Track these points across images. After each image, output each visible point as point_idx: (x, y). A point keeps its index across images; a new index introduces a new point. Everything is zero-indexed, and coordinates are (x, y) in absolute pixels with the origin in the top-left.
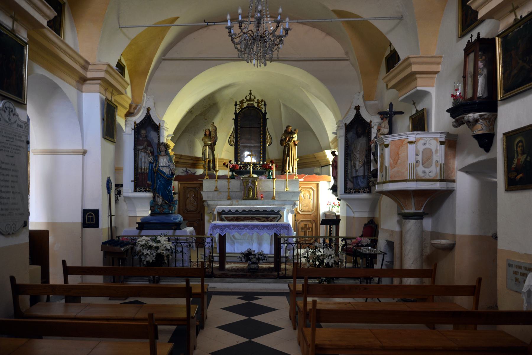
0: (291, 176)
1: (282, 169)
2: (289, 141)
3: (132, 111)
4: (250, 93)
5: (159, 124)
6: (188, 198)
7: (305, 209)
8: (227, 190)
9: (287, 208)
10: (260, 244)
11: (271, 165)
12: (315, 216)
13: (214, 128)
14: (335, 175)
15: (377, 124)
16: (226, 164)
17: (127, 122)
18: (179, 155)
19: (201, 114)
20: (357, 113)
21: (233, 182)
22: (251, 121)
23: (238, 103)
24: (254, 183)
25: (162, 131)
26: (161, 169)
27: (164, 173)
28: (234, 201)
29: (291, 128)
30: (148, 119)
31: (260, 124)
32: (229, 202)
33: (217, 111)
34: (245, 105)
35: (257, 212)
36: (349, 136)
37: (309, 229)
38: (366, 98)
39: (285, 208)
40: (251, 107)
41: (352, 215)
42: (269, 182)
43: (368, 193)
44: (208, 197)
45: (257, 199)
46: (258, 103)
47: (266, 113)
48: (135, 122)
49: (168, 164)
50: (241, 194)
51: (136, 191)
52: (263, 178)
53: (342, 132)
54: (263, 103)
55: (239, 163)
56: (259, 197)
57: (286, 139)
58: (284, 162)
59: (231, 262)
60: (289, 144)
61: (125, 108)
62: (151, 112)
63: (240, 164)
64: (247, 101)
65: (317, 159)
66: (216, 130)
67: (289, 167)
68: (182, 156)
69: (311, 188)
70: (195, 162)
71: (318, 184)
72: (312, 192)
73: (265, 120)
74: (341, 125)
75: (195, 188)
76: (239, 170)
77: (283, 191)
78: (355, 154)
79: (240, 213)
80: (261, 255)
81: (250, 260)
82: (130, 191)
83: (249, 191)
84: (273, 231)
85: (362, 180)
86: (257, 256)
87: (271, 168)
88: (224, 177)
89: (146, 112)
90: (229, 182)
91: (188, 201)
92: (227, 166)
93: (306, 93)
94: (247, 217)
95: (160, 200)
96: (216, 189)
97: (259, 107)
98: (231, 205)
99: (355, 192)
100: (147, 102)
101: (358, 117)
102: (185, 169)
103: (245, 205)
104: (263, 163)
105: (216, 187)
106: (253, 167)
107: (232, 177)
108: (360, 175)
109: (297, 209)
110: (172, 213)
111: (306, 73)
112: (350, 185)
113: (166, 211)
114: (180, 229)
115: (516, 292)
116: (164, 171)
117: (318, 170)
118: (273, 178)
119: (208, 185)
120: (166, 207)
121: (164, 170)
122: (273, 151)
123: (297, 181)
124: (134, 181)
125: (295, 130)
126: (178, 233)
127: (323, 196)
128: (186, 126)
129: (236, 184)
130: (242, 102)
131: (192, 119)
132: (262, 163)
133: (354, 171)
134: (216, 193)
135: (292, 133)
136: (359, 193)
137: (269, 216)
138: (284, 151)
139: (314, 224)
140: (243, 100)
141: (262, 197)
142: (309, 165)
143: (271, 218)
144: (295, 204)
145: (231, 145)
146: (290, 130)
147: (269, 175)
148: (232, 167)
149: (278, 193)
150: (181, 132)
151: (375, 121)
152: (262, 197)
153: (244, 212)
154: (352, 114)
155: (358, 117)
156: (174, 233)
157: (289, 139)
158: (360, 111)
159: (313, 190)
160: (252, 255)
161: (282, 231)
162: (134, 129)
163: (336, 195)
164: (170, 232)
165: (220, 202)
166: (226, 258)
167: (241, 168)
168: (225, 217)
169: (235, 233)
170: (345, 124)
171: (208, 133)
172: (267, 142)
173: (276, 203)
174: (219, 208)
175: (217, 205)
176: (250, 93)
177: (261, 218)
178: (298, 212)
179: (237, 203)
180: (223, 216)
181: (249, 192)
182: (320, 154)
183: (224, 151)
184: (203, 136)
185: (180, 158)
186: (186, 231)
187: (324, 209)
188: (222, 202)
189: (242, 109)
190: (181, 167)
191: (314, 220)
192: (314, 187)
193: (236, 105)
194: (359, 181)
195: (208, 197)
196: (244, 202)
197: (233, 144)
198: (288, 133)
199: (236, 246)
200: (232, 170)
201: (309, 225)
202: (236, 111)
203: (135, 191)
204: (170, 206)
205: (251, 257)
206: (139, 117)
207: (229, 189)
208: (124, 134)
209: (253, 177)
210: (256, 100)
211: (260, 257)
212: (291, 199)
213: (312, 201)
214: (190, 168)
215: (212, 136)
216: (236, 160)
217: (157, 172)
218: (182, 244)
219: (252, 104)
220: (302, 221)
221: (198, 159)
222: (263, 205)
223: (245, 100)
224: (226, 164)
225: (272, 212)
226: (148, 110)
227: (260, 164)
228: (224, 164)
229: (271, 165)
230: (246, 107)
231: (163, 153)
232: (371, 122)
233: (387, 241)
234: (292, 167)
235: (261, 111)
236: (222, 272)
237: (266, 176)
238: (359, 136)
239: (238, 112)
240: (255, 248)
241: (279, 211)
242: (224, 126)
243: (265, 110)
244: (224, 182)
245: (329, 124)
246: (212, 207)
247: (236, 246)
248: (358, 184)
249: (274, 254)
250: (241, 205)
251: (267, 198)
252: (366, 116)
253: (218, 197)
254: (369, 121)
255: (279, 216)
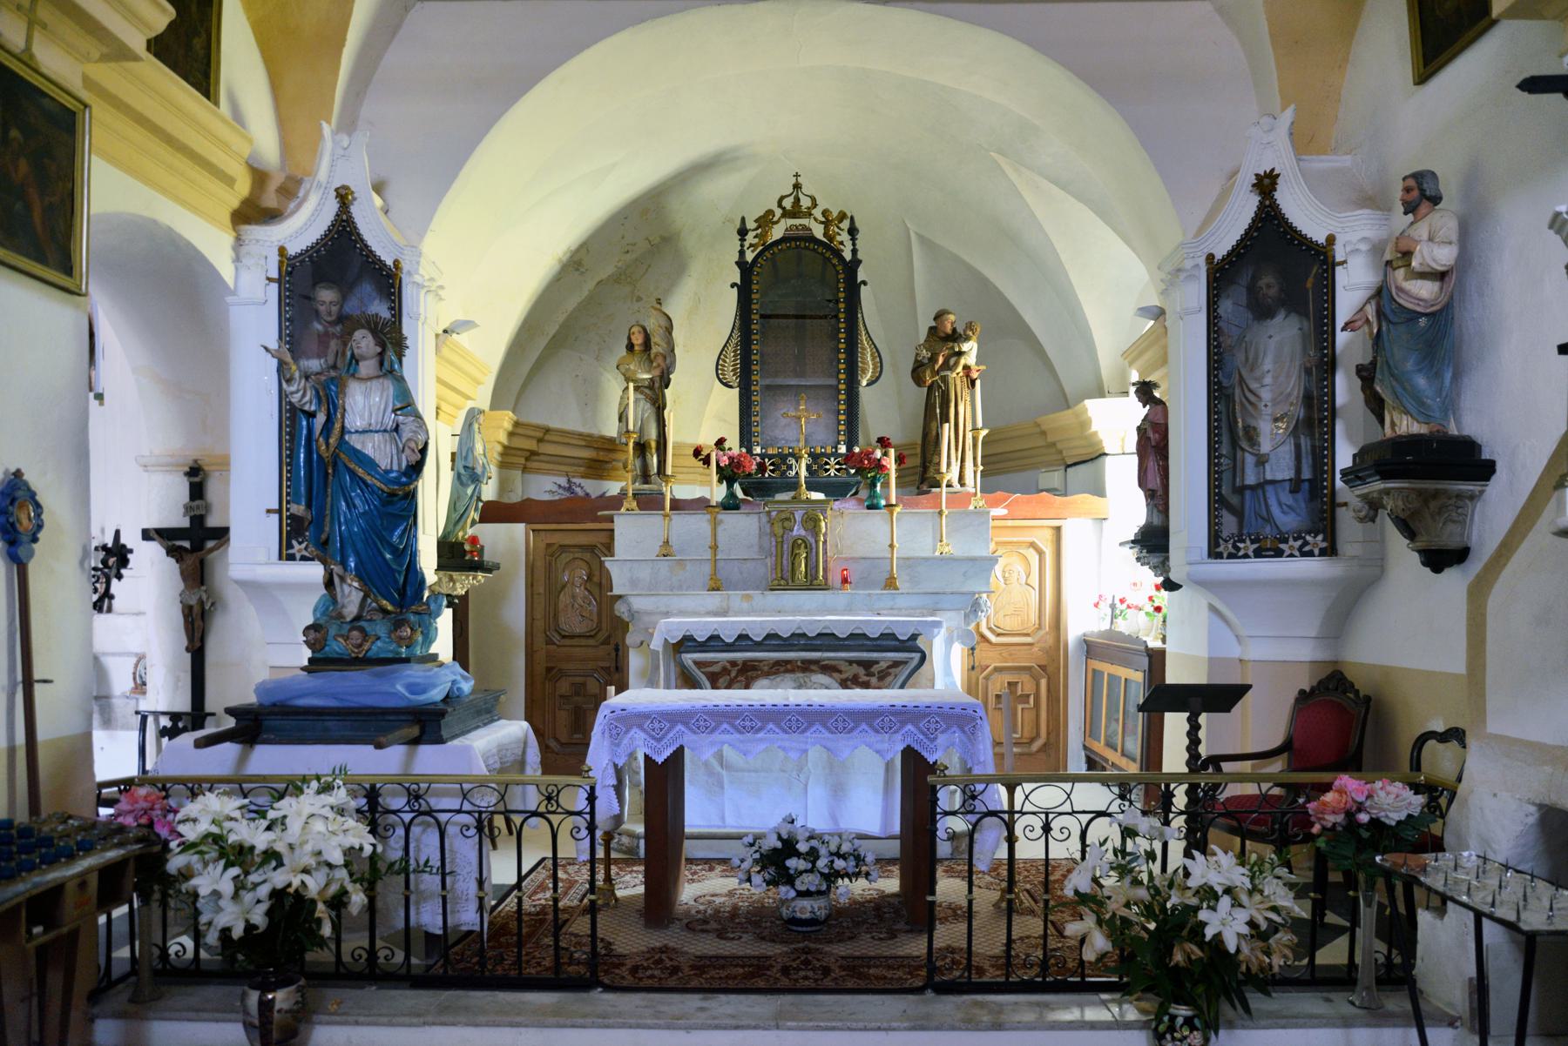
0: (959, 500)
1: (922, 474)
2: (947, 366)
3: (270, 200)
4: (797, 186)
5: (396, 263)
6: (564, 587)
7: (1009, 624)
8: (708, 555)
9: (949, 620)
10: (838, 791)
11: (878, 454)
12: (1046, 651)
13: (663, 322)
14: (1154, 482)
15: (1364, 247)
16: (705, 453)
17: (244, 250)
18: (537, 427)
19: (618, 279)
20: (1261, 207)
21: (730, 519)
22: (800, 293)
23: (751, 225)
24: (812, 523)
25: (408, 292)
26: (355, 441)
27: (368, 463)
28: (735, 597)
29: (952, 317)
30: (343, 234)
31: (837, 301)
32: (714, 600)
33: (680, 268)
34: (777, 233)
35: (827, 640)
36: (1226, 307)
37: (1024, 698)
38: (1304, 141)
39: (938, 624)
40: (799, 241)
41: (1235, 651)
42: (876, 519)
43: (1323, 553)
44: (634, 583)
45: (825, 587)
46: (827, 224)
47: (856, 262)
48: (282, 251)
49: (390, 420)
50: (765, 569)
51: (291, 558)
52: (848, 506)
53: (1196, 293)
54: (845, 225)
55: (758, 450)
56: (835, 578)
57: (933, 359)
58: (930, 444)
59: (710, 863)
60: (945, 379)
61: (229, 181)
62: (356, 211)
63: (762, 456)
64: (786, 214)
65: (1050, 439)
66: (669, 329)
67: (949, 464)
68: (547, 430)
69: (1032, 545)
70: (600, 456)
71: (1058, 529)
72: (1034, 558)
73: (853, 288)
74: (1188, 264)
75: (591, 548)
76: (751, 479)
77: (928, 554)
78: (1254, 385)
79: (758, 646)
80: (843, 857)
81: (790, 880)
82: (262, 558)
83: (794, 556)
84: (898, 737)
85: (1287, 498)
86: (821, 863)
87: (879, 466)
88: (702, 504)
89: (332, 206)
90: (715, 524)
91: (564, 599)
92: (707, 461)
93: (1013, 176)
94: (787, 662)
95: (351, 596)
96: (666, 550)
97: (831, 239)
98: (724, 613)
99: (1258, 554)
100: (338, 161)
101: (1270, 227)
102: (563, 481)
103: (793, 613)
104: (849, 449)
105: (667, 542)
106: (809, 467)
107: (730, 504)
108: (1279, 477)
109: (978, 625)
110: (407, 660)
111: (1026, 51)
112: (1229, 523)
113: (378, 648)
114: (440, 740)
115: (92, 335)
116: (369, 450)
117: (1055, 478)
118: (889, 506)
119: (634, 535)
120: (381, 628)
121: (372, 447)
122: (886, 407)
123: (981, 514)
124: (280, 511)
125: (970, 326)
126: (430, 759)
127: (1085, 570)
128: (561, 318)
129: (744, 528)
130: (766, 221)
131: (586, 293)
132: (843, 449)
133: (1250, 460)
134: (664, 567)
135: (955, 337)
136: (1279, 553)
137: (875, 655)
138: (929, 407)
139: (1043, 682)
140: (770, 212)
141: (845, 581)
142: (1037, 458)
143: (883, 665)
144: (976, 607)
145: (727, 385)
146: (949, 329)
147: (873, 495)
148: (725, 461)
149: (910, 562)
150: (542, 342)
151: (1354, 237)
152: (845, 581)
153: (772, 640)
154: (1242, 212)
155: (1270, 227)
156: (410, 758)
157: (946, 362)
158: (1277, 195)
159: (1041, 553)
160: (798, 855)
161: (942, 739)
162: (279, 281)
163: (1162, 567)
164: (366, 760)
165: (677, 602)
166: (687, 843)
167: (762, 468)
168: (698, 664)
169: (728, 745)
170: (1210, 257)
171: (638, 340)
172: (864, 371)
173: (901, 602)
174: (671, 627)
175: (667, 614)
176: (797, 186)
177: (844, 666)
178: (983, 637)
179: (745, 605)
180: (689, 658)
181: (796, 566)
182: (1065, 417)
183: (703, 411)
184: (623, 352)
185: (540, 440)
186: (468, 749)
187: (1082, 622)
188: (687, 602)
189: (767, 248)
190: (548, 472)
191: (1043, 667)
192: (1045, 541)
193: (743, 232)
194: (1272, 502)
195: (634, 583)
196: (773, 598)
197: (734, 380)
198: (944, 338)
199: (731, 803)
200: (728, 475)
201: (1026, 685)
202: (742, 253)
203: (286, 555)
204: (398, 624)
205: (793, 863)
206: (303, 227)
207: (714, 548)
208: (229, 299)
209: (808, 501)
210: (817, 213)
211: (839, 864)
212: (962, 585)
213: (1034, 596)
214: (583, 477)
215: (654, 350)
216: (746, 437)
217: (335, 457)
218: (443, 817)
219: (805, 228)
220: (997, 670)
221: (609, 446)
222: (849, 611)
223: (778, 212)
224: (705, 453)
225: (888, 641)
226: (344, 197)
227: (836, 455)
228: (697, 452)
229: (878, 454)
230: (783, 240)
231: (367, 367)
232: (1331, 240)
233: (1541, 806)
234: (959, 467)
235: (838, 253)
236: (656, 939)
237: (861, 501)
238: (1262, 311)
239: (750, 256)
240: (814, 817)
241: (914, 637)
242: (703, 317)
243: (854, 251)
244: (698, 524)
245: (1114, 290)
246: (646, 619)
247: (731, 803)
248: (1269, 519)
249: (902, 837)
250: (761, 612)
251: (867, 583)
252: (1307, 215)
253: (672, 577)
254: (1319, 237)
255: (917, 656)
